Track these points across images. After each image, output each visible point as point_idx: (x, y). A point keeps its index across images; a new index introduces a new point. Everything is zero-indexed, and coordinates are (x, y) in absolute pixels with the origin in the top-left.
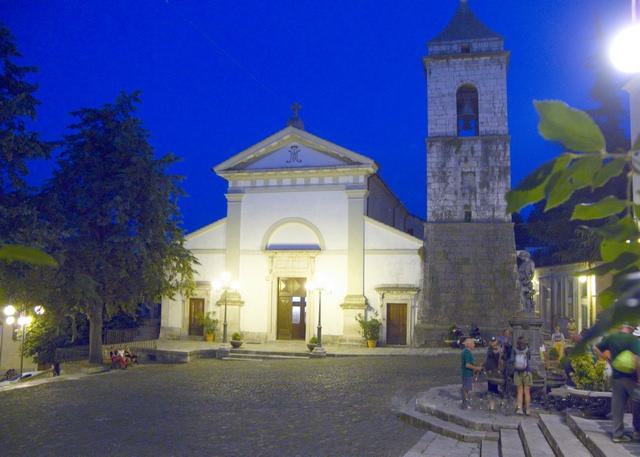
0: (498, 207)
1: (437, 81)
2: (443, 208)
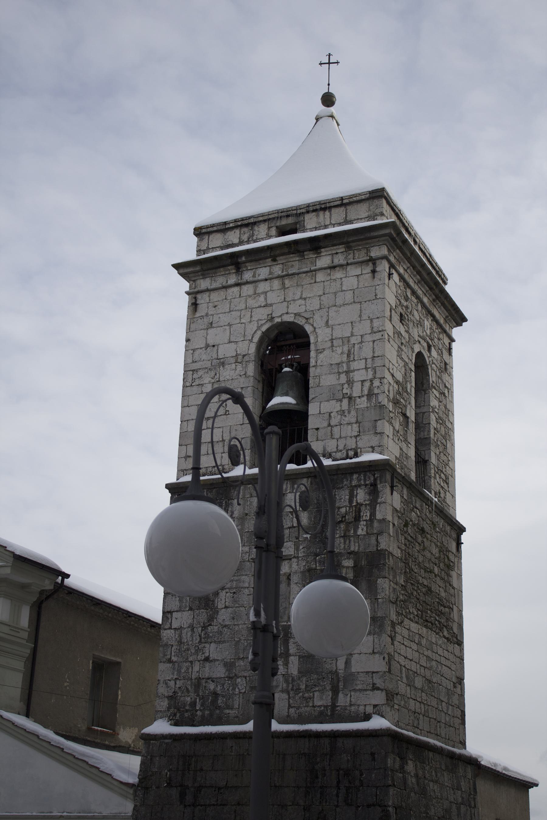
0: (350, 678)
1: (211, 325)
2: (198, 683)
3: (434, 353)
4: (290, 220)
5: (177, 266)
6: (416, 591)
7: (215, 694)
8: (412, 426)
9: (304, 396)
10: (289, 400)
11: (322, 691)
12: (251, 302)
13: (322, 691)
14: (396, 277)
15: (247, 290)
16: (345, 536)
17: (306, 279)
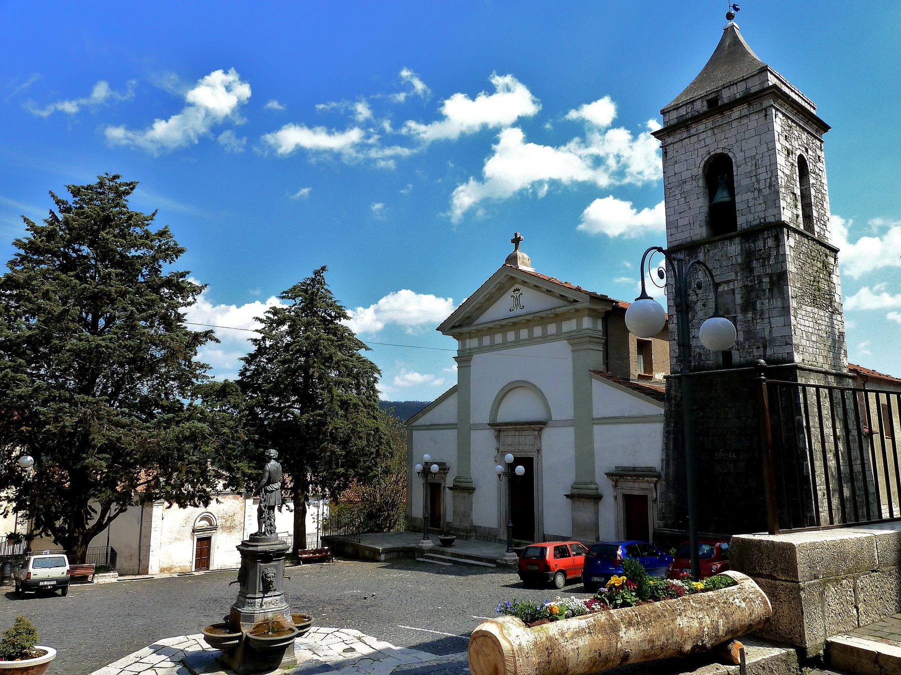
0: (772, 341)
3: (810, 152)
7: (700, 354)
8: (799, 198)
9: (732, 194)
12: (697, 146)
14: (780, 115)
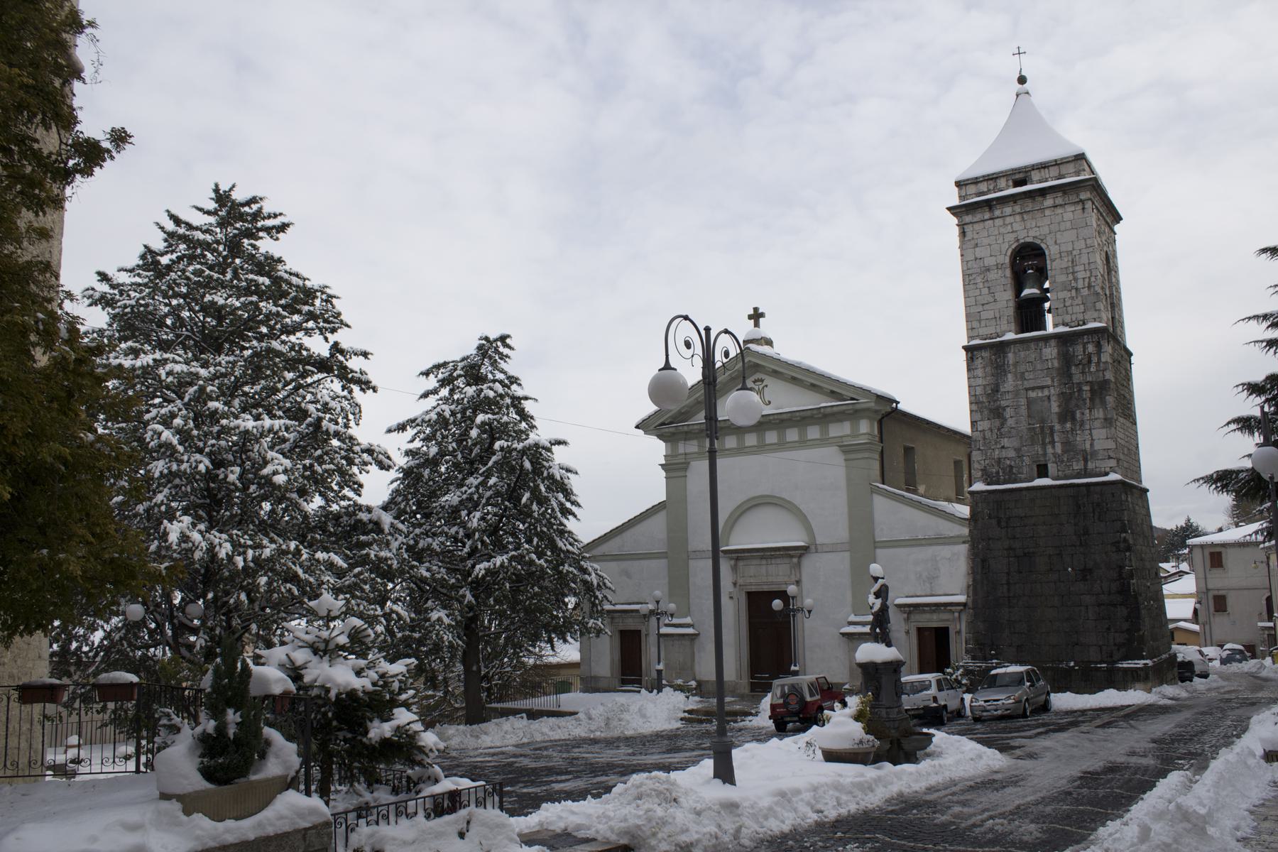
0: (1094, 454)
2: (999, 461)
4: (1021, 176)
5: (949, 209)
6: (483, 484)
10: (1035, 291)
11: (1078, 461)
12: (1002, 230)
13: (1078, 461)
15: (998, 222)
16: (1083, 373)
17: (1039, 215)
